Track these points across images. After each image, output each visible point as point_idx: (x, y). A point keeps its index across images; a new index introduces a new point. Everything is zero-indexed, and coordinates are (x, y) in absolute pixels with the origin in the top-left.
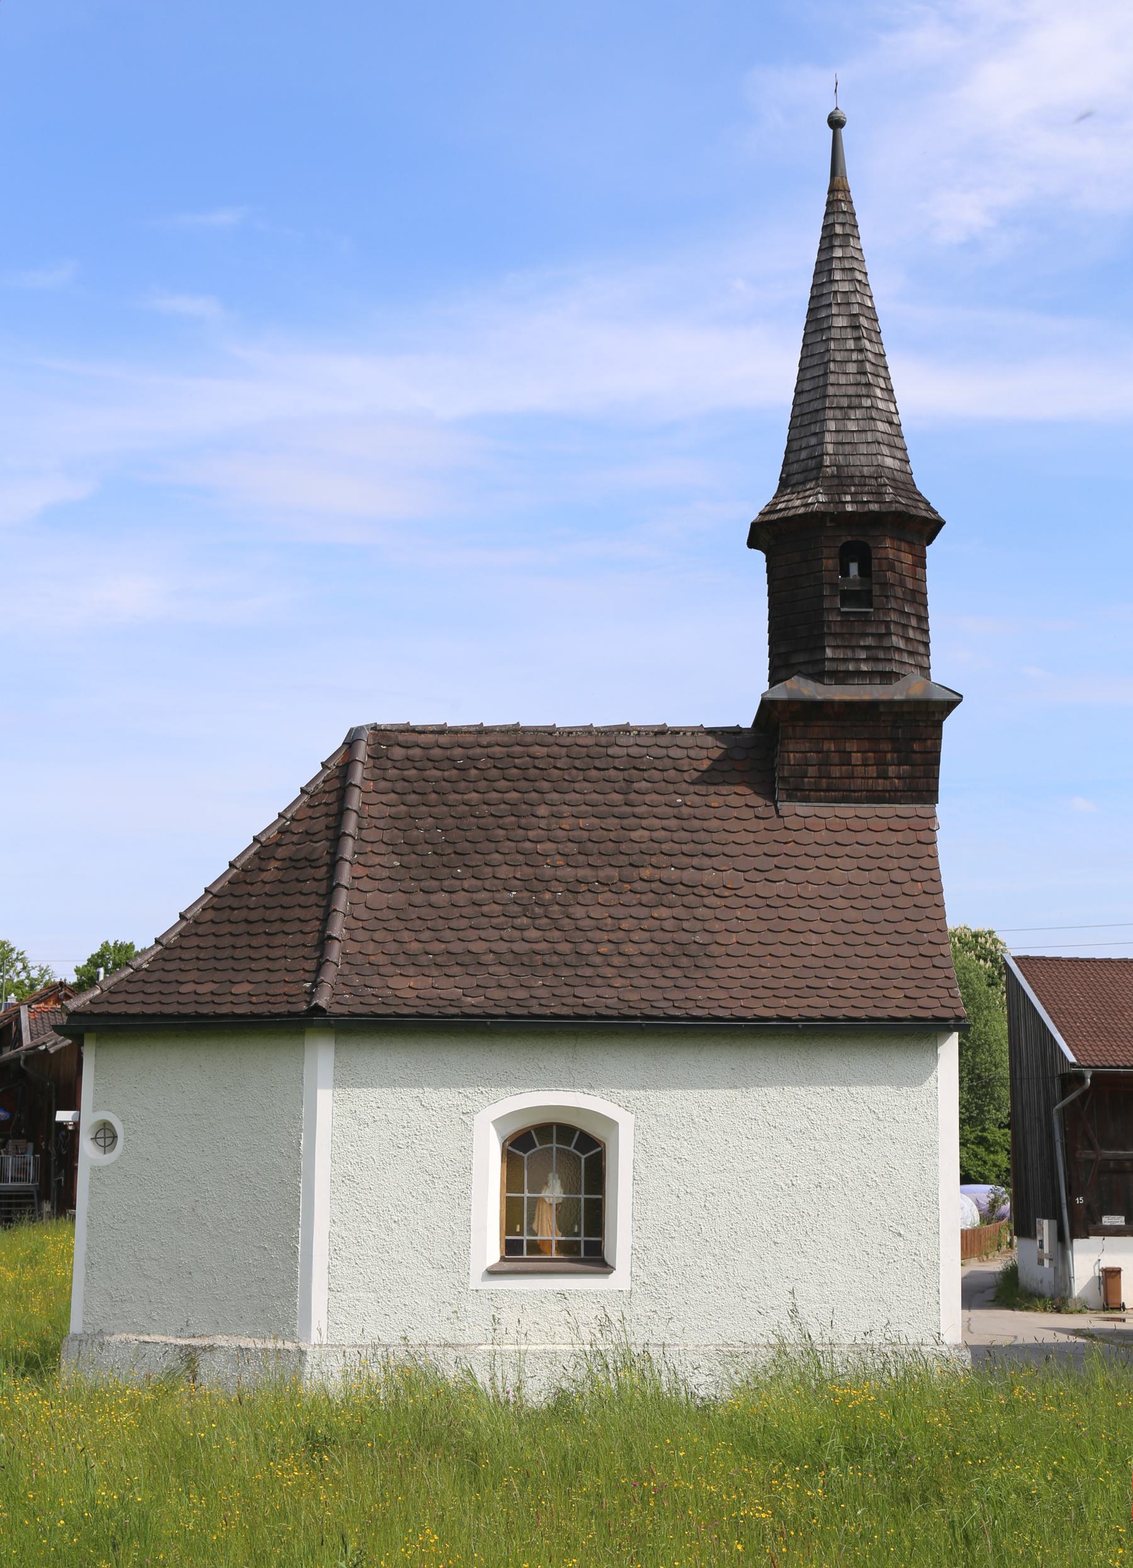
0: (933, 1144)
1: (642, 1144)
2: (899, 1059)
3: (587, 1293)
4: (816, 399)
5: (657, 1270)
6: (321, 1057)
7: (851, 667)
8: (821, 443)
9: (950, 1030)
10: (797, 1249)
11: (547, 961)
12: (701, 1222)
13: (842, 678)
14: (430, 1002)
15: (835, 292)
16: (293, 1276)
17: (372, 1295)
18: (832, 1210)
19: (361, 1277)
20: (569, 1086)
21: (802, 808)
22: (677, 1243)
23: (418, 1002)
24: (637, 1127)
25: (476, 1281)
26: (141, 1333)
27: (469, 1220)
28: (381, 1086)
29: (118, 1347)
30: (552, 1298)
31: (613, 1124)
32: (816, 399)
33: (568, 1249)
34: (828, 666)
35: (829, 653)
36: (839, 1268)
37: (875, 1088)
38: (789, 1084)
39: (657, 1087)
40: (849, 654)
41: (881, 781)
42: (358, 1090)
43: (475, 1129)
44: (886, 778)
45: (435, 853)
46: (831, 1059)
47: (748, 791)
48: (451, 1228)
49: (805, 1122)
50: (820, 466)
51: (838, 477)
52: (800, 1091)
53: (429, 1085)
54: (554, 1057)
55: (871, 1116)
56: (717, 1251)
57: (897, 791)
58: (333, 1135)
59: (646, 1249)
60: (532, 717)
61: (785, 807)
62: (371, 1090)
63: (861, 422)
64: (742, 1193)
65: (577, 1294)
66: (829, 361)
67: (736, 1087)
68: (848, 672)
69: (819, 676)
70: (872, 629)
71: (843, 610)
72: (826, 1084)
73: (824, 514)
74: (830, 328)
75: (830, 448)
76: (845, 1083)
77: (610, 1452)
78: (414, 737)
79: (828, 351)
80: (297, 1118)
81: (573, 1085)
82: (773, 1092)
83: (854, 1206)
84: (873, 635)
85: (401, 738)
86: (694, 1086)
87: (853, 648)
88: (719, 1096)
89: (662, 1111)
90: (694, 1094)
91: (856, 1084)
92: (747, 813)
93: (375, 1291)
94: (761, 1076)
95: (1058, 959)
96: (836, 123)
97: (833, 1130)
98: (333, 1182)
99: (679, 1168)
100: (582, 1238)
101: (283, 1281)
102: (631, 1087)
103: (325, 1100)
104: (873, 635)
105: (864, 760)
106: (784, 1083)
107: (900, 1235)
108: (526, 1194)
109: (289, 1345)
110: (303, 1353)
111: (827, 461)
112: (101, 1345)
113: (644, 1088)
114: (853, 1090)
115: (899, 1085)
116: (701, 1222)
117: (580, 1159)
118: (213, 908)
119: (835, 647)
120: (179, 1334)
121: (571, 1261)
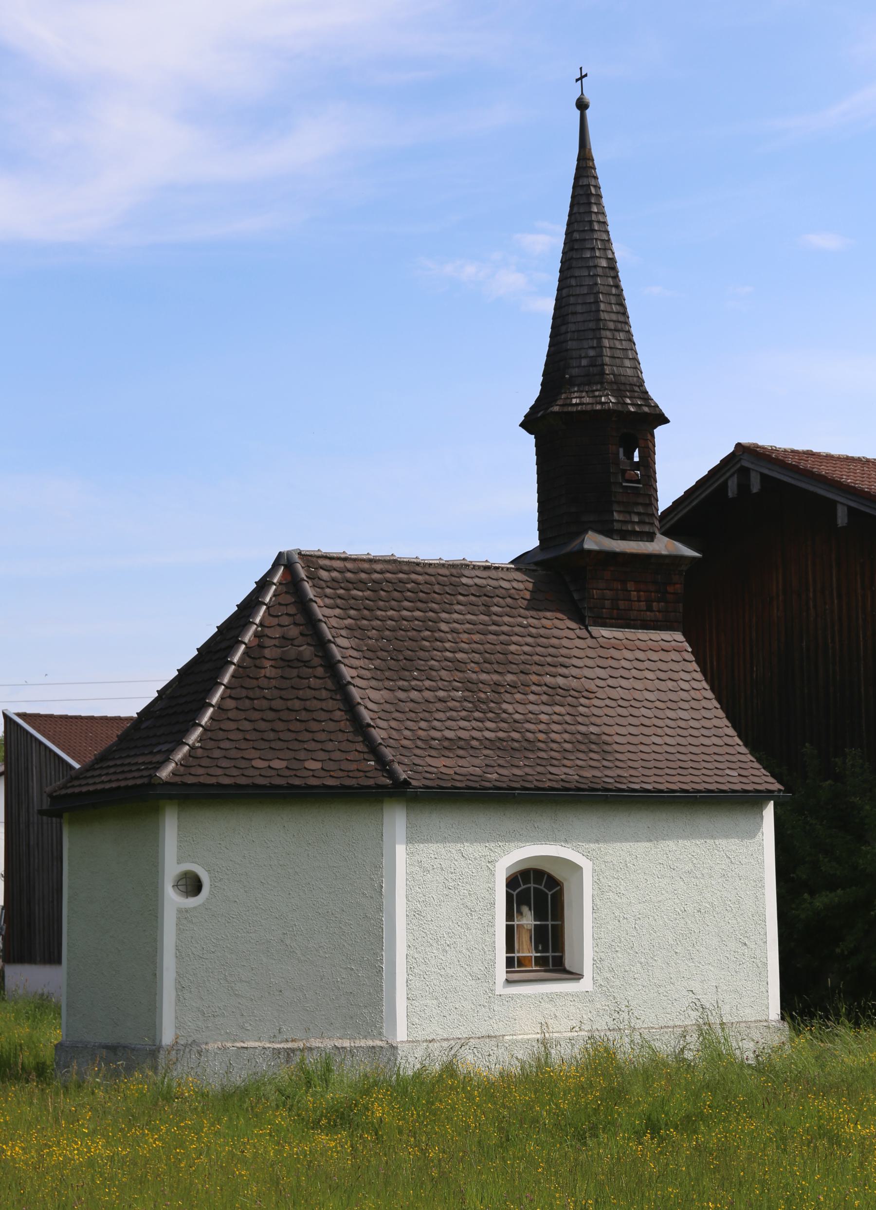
0: (762, 880)
1: (596, 882)
2: (742, 820)
3: (567, 994)
4: (590, 321)
5: (608, 975)
6: (397, 820)
7: (630, 528)
8: (601, 355)
9: (769, 799)
10: (688, 957)
11: (248, 737)
12: (633, 939)
13: (625, 535)
14: (332, 773)
15: (596, 239)
16: (379, 989)
17: (435, 1002)
18: (707, 928)
19: (427, 989)
20: (553, 841)
21: (605, 632)
22: (619, 955)
23: (288, 773)
24: (594, 871)
25: (500, 988)
26: (235, 1041)
27: (494, 942)
28: (437, 842)
29: (216, 1053)
30: (545, 998)
31: (577, 869)
32: (590, 321)
33: (541, 962)
34: (617, 526)
35: (616, 516)
36: (712, 969)
37: (729, 841)
38: (681, 838)
39: (605, 841)
40: (628, 518)
41: (648, 613)
42: (422, 845)
43: (496, 874)
44: (652, 611)
45: (392, 658)
46: (704, 820)
47: (565, 617)
48: (483, 949)
49: (691, 865)
50: (602, 373)
51: (615, 383)
52: (687, 843)
53: (467, 841)
54: (543, 820)
55: (728, 860)
56: (643, 960)
57: (657, 621)
58: (407, 880)
59: (601, 960)
60: (404, 551)
61: (596, 631)
62: (431, 845)
63: (624, 342)
64: (656, 917)
65: (559, 995)
66: (599, 293)
67: (651, 841)
68: (628, 531)
69: (609, 533)
70: (640, 500)
71: (624, 484)
72: (701, 838)
73: (614, 411)
74: (596, 267)
75: (607, 360)
76: (713, 837)
77: (605, 1106)
78: (327, 562)
79: (596, 284)
80: (378, 867)
81: (555, 840)
82: (671, 844)
83: (720, 925)
84: (641, 504)
85: (322, 562)
86: (627, 840)
87: (630, 513)
88: (641, 847)
89: (608, 858)
90: (626, 846)
91: (719, 838)
92: (571, 634)
93: (436, 999)
94: (665, 832)
95: (51, 717)
96: (582, 105)
97: (706, 871)
98: (407, 916)
99: (619, 900)
100: (550, 954)
101: (370, 994)
102: (589, 841)
103: (401, 851)
104: (641, 504)
105: (639, 597)
106: (679, 837)
107: (745, 944)
108: (550, 923)
109: (378, 1043)
110: (394, 1048)
111: (607, 370)
112: (200, 1053)
113: (597, 841)
114: (717, 842)
115: (743, 839)
116: (633, 939)
117: (547, 895)
118: (230, 697)
119: (619, 512)
120: (273, 1039)
121: (545, 971)
